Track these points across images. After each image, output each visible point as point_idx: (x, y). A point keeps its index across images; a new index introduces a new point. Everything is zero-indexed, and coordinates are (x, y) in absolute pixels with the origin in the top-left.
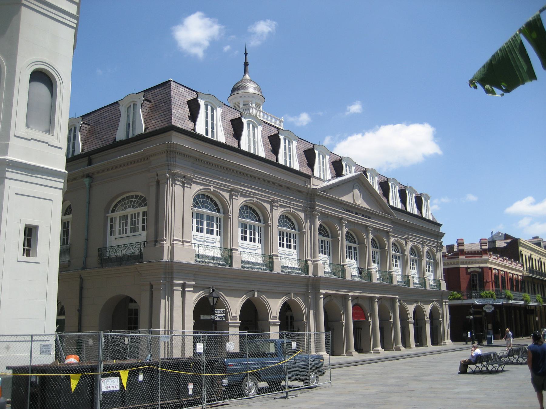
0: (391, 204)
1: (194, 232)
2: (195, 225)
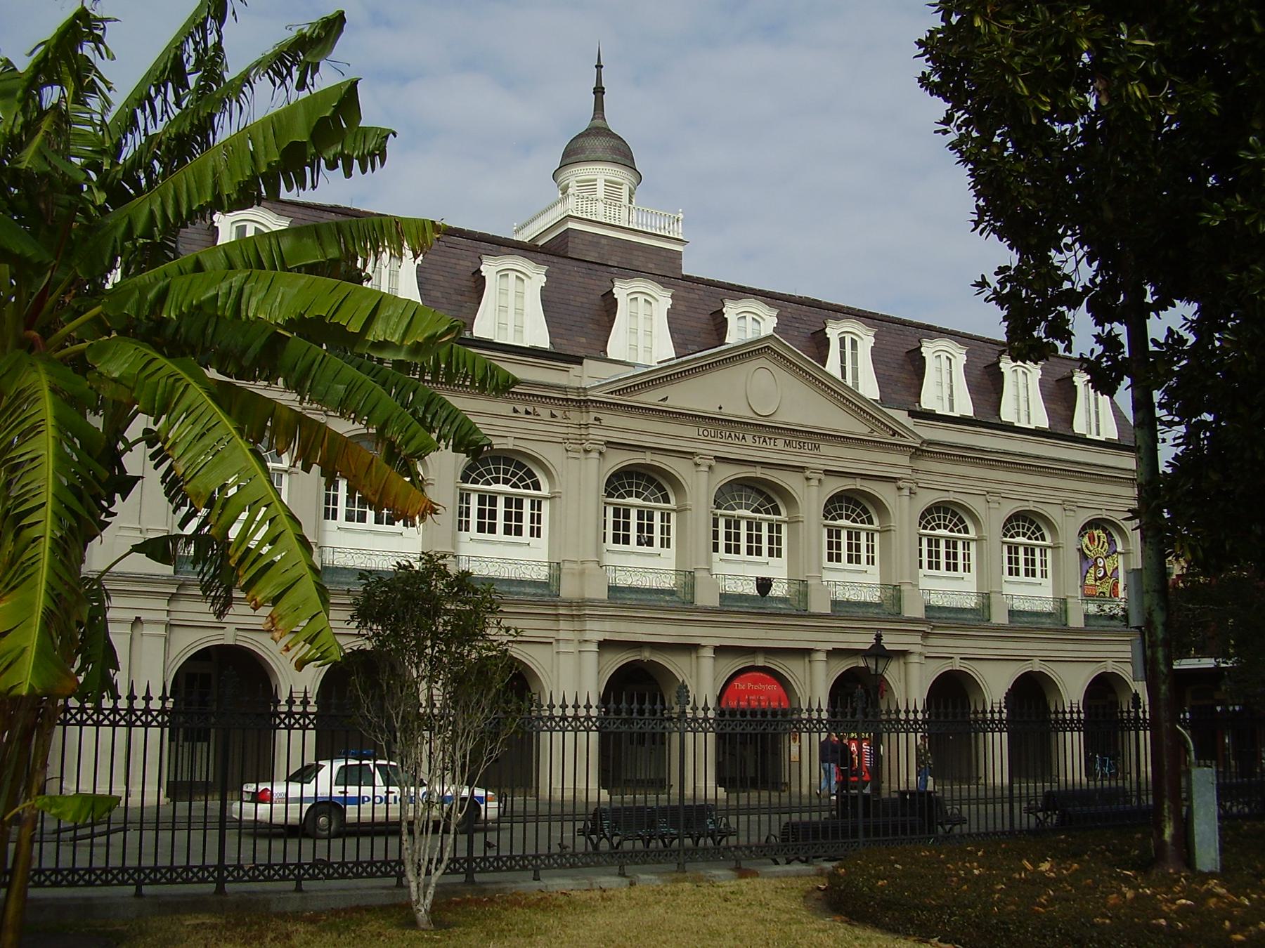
1: (1006, 576)
2: (610, 532)
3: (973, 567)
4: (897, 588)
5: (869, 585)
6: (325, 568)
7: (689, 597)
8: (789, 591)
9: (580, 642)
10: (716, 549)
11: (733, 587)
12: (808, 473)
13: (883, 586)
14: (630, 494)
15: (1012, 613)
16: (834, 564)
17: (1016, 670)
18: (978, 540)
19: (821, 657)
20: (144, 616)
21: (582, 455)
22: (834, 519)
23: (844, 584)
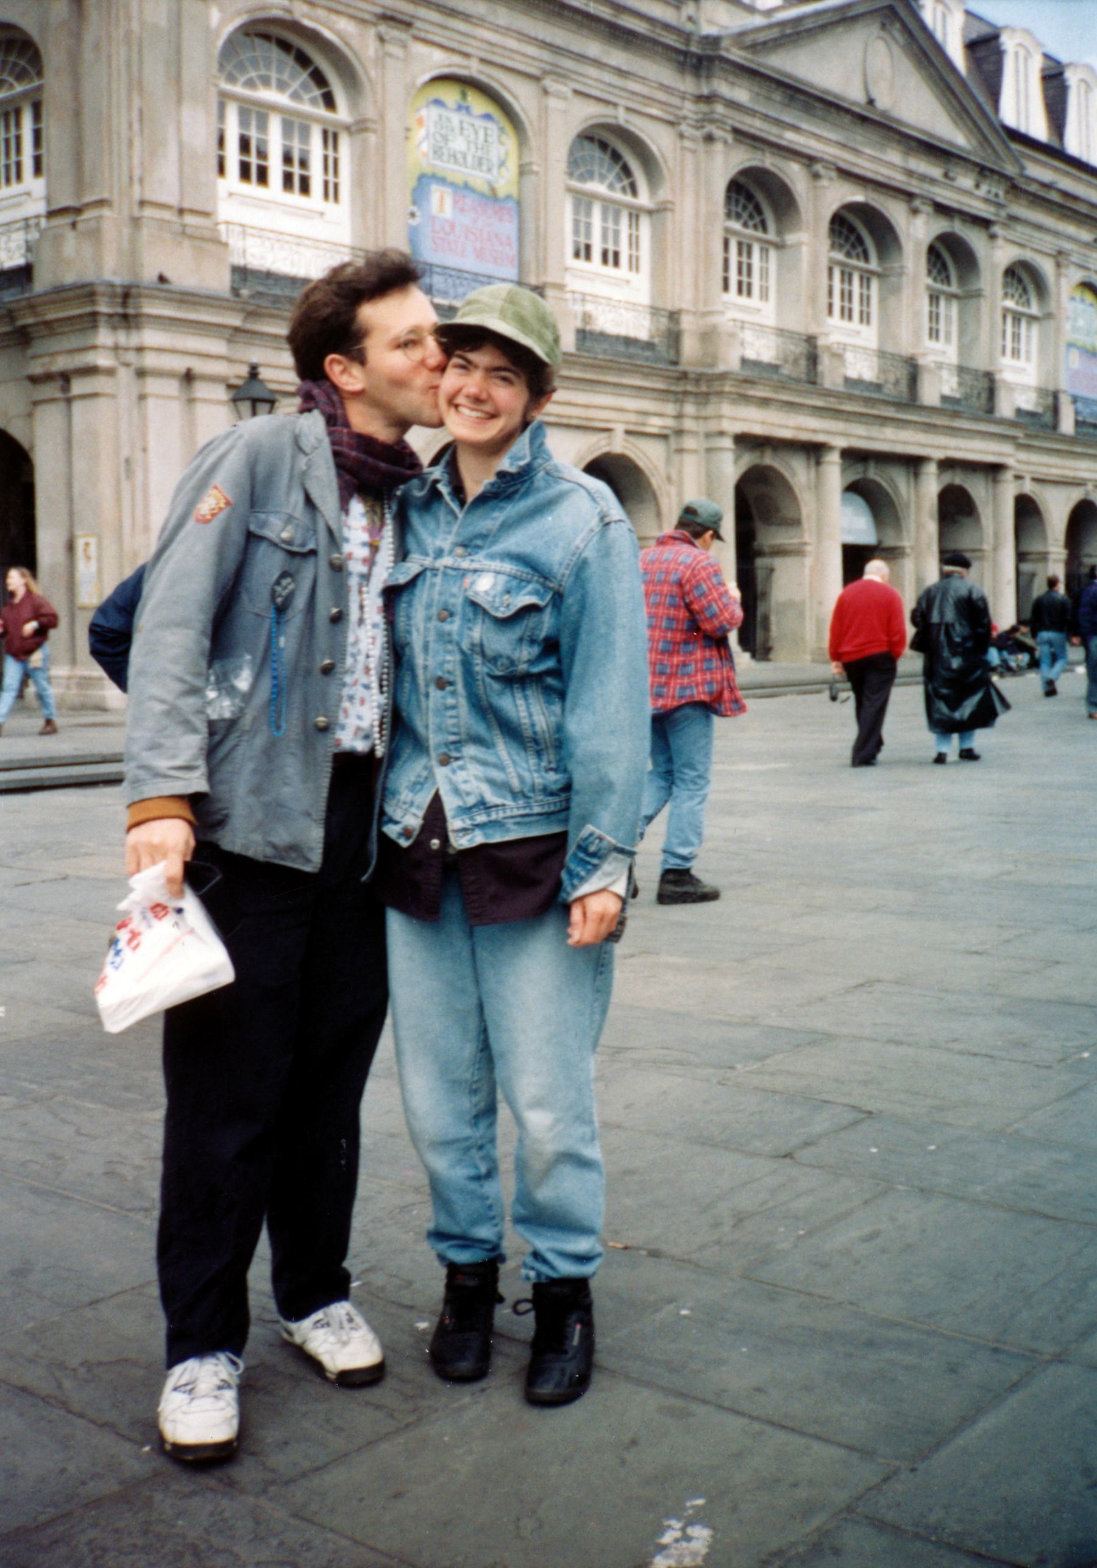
0: (1009, 113)
3: (772, 294)
4: (674, 316)
5: (633, 306)
6: (592, 333)
7: (672, 355)
8: (1037, 404)
9: (708, 435)
10: (726, 287)
11: (608, 322)
12: (818, 167)
13: (1042, 392)
14: (266, 82)
15: (583, 335)
16: (581, 264)
17: (1075, 495)
18: (359, 128)
19: (834, 458)
20: (200, 366)
21: (701, 147)
22: (582, 178)
23: (261, 232)
